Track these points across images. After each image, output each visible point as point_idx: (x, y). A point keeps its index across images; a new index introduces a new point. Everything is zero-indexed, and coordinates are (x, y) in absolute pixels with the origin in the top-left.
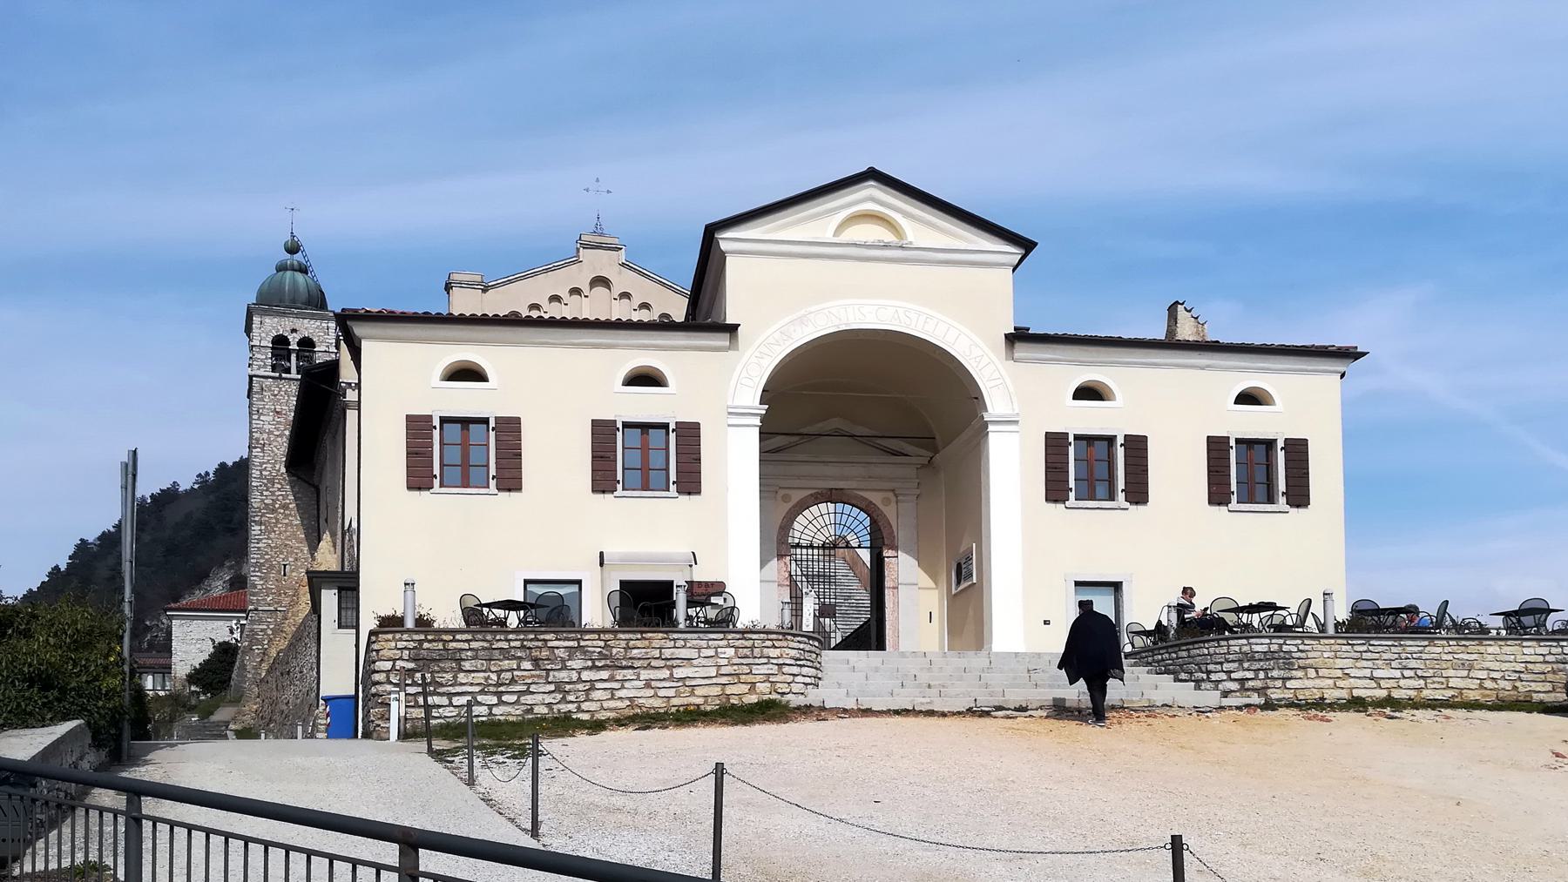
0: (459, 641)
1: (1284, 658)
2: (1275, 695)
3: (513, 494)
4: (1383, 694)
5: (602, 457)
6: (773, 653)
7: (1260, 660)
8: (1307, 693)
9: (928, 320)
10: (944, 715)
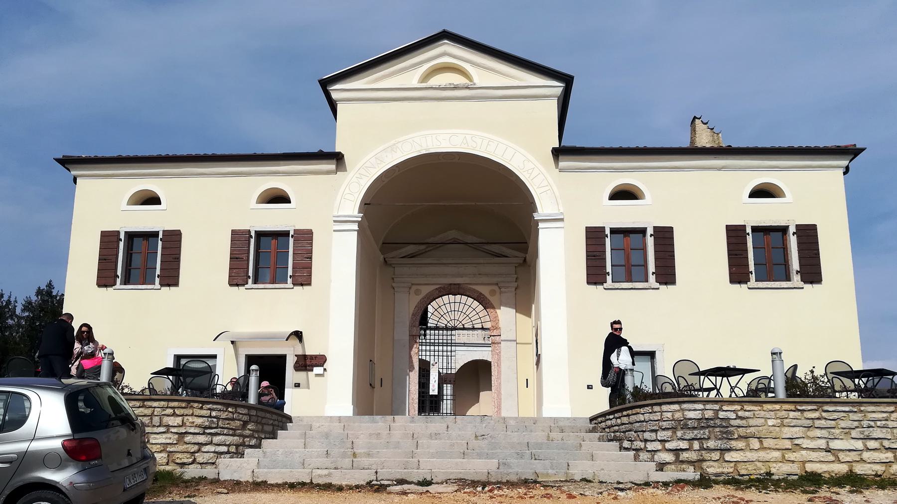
1: (721, 426)
2: (712, 469)
3: (172, 288)
4: (842, 469)
5: (237, 258)
6: (172, 421)
7: (694, 428)
8: (750, 467)
9: (490, 143)
10: (340, 489)
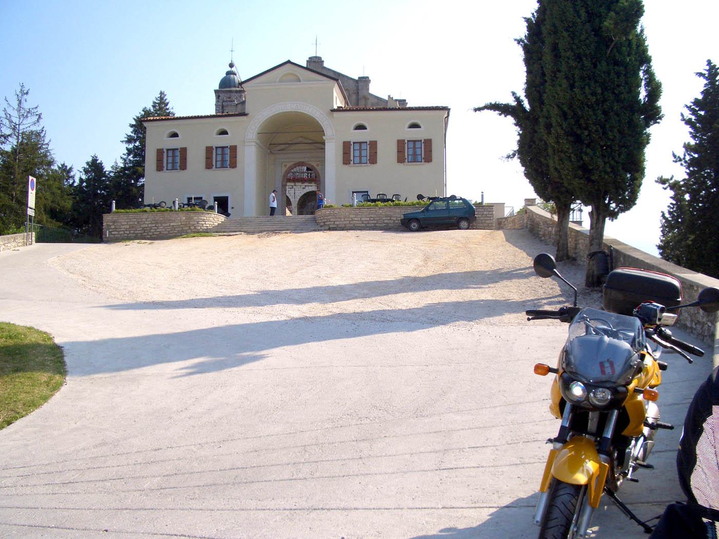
0: (348, 221)
